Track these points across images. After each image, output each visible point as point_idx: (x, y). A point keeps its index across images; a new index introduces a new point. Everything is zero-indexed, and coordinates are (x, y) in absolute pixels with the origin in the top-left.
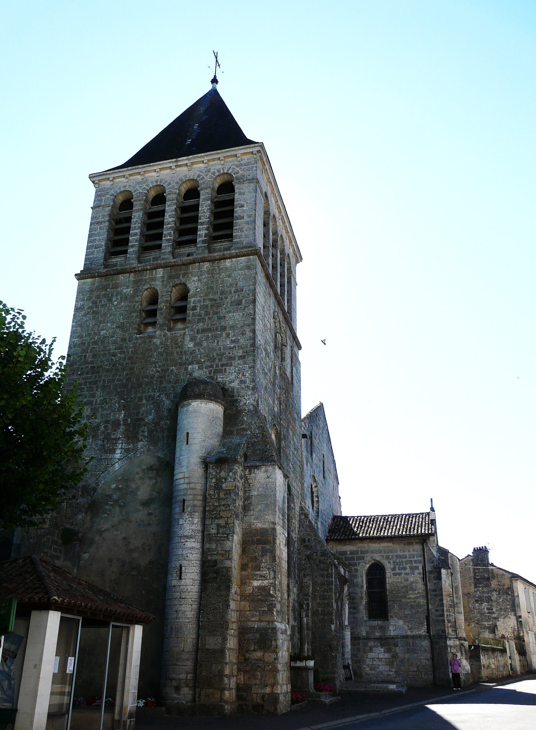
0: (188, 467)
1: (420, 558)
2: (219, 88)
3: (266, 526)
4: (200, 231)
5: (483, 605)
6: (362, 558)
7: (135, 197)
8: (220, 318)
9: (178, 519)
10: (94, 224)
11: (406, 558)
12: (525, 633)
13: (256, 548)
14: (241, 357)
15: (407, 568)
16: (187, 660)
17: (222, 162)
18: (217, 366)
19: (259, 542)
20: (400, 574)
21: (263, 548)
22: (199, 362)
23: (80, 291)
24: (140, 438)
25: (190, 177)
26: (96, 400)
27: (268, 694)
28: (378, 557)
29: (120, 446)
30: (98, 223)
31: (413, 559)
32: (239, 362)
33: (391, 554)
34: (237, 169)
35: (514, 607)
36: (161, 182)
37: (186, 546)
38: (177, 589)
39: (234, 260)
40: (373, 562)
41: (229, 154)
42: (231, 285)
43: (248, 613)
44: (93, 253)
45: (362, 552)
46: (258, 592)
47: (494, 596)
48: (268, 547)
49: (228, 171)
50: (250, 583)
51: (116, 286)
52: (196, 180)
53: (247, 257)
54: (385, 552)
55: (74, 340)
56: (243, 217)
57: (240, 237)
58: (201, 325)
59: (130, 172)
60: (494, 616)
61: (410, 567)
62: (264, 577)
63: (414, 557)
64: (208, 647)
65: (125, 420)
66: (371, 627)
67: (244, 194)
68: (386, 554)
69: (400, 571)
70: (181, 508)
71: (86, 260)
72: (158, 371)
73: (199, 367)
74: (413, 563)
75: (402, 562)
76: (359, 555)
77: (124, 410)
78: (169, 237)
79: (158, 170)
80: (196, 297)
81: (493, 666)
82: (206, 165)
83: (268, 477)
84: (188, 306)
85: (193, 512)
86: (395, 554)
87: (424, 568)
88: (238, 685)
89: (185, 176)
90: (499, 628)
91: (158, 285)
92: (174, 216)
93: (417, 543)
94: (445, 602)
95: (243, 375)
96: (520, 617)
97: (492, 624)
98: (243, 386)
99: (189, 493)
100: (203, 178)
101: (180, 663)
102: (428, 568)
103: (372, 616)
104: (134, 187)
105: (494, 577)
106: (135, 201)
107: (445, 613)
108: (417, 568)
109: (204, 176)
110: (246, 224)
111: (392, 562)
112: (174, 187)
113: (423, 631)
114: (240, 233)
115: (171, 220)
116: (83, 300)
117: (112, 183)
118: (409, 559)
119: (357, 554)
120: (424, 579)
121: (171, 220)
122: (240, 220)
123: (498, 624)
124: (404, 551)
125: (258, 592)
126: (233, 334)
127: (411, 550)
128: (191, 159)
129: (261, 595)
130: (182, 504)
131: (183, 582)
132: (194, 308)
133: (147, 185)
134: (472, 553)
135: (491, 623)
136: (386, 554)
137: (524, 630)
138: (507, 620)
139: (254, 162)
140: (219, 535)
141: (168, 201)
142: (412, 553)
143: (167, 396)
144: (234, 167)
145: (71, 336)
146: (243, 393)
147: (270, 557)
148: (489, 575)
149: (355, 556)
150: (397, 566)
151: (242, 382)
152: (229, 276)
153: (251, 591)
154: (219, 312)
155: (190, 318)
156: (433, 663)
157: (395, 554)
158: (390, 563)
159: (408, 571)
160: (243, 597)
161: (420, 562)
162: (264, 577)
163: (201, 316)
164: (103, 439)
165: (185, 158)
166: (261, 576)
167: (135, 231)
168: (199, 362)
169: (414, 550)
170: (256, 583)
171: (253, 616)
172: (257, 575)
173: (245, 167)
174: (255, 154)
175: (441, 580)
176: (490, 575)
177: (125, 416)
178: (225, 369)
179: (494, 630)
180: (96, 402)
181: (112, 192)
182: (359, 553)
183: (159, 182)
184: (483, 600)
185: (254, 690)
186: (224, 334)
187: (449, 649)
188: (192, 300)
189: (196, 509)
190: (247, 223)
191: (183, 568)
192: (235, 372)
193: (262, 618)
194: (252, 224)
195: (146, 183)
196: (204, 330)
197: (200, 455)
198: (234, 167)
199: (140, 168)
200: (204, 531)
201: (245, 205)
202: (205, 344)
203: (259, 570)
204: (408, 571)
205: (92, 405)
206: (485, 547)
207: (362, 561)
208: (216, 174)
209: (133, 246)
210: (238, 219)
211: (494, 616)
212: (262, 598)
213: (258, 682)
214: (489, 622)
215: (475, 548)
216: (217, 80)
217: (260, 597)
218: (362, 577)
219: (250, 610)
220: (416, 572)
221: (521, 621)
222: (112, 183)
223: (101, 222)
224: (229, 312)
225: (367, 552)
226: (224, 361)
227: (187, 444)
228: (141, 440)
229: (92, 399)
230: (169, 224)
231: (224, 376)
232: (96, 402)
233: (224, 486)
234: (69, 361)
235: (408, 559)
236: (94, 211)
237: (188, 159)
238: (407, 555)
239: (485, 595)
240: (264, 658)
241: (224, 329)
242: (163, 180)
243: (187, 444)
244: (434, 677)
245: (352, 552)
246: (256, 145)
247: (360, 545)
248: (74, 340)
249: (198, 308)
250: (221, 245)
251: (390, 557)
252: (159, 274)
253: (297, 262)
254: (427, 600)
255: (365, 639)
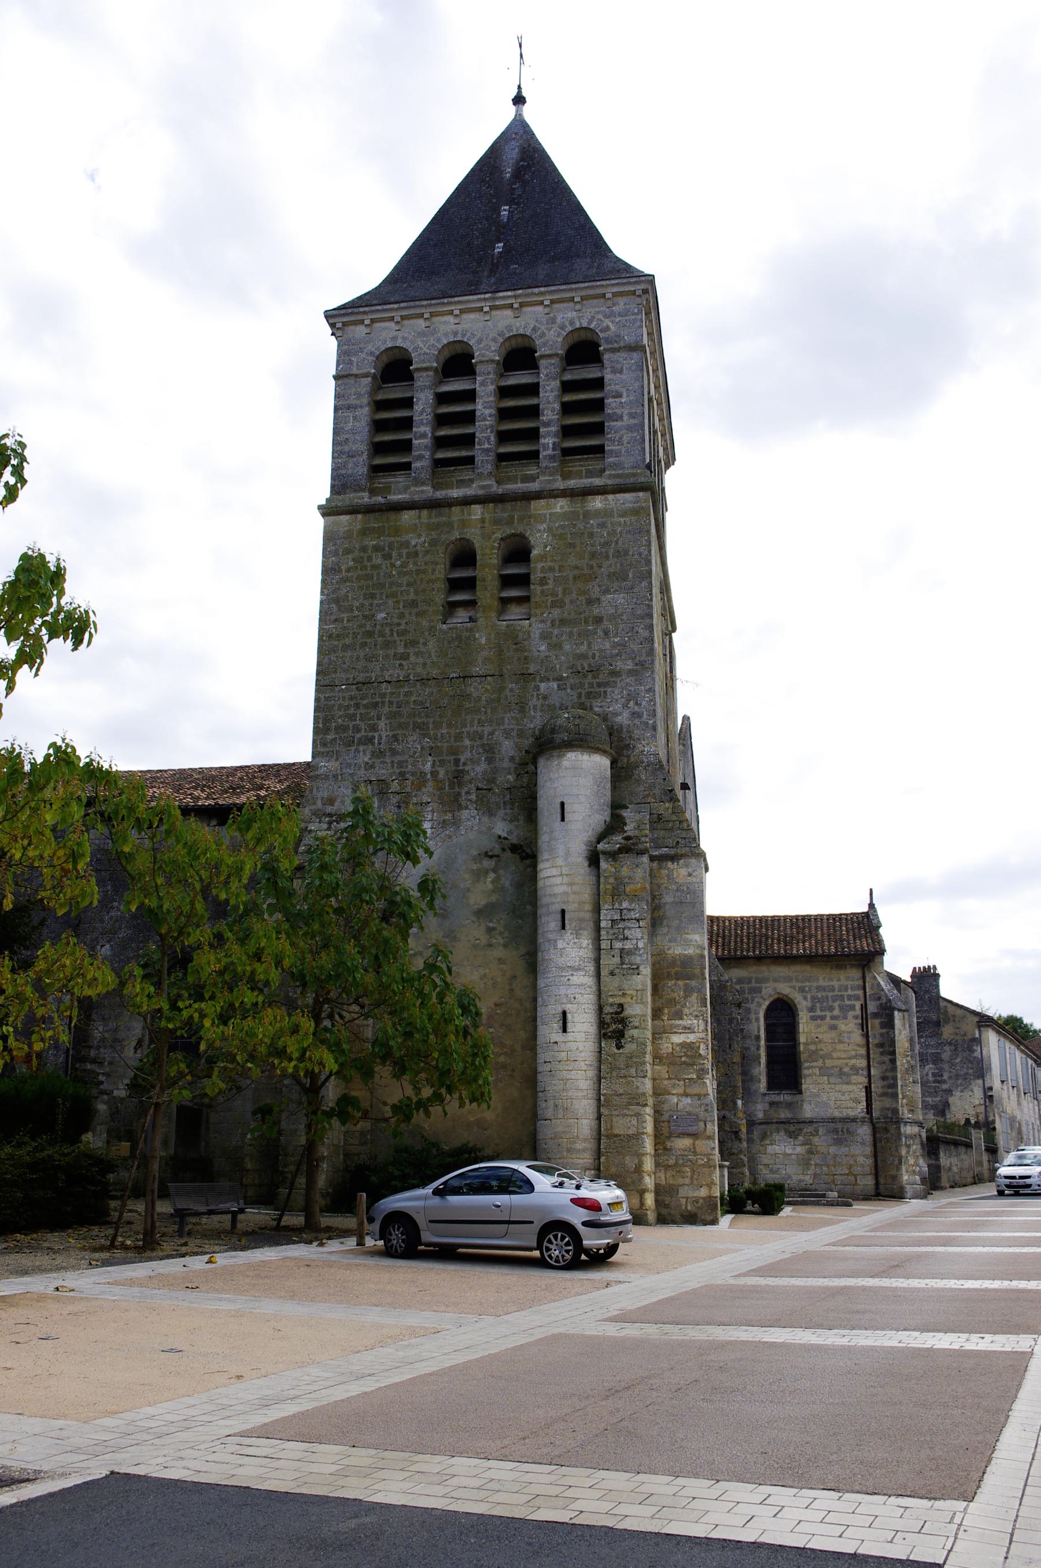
0: (566, 859)
1: (856, 992)
2: (530, 114)
3: (690, 951)
4: (545, 437)
5: (927, 1067)
6: (759, 990)
7: (416, 362)
8: (590, 602)
9: (555, 941)
10: (342, 409)
11: (833, 990)
12: (997, 1116)
13: (675, 985)
14: (630, 673)
15: (834, 1009)
16: (584, 1150)
17: (578, 307)
18: (591, 685)
19: (678, 977)
20: (823, 1018)
21: (686, 985)
22: (560, 679)
23: (329, 538)
24: (464, 803)
25: (517, 330)
26: (380, 735)
27: (704, 1199)
28: (785, 989)
29: (429, 817)
30: (349, 407)
31: (845, 993)
32: (628, 680)
33: (807, 984)
34: (607, 322)
35: (981, 1070)
36: (464, 335)
37: (571, 982)
38: (563, 1047)
39: (610, 497)
40: (776, 996)
41: (591, 292)
42: (607, 544)
43: (666, 1082)
44: (345, 465)
45: (758, 981)
46: (681, 1052)
47: (946, 1053)
48: (693, 983)
49: (590, 322)
50: (667, 1037)
51: (397, 531)
52: (529, 337)
53: (634, 494)
54: (797, 980)
55: (327, 627)
56: (621, 417)
57: (618, 454)
58: (556, 613)
59: (405, 313)
60: (945, 1086)
61: (839, 1006)
62: (689, 1028)
63: (846, 990)
64: (616, 1131)
65: (434, 774)
66: (772, 1104)
67: (621, 372)
68: (799, 985)
69: (823, 1014)
70: (560, 924)
71: (333, 478)
72: (487, 690)
73: (558, 686)
74: (846, 1000)
75: (827, 997)
76: (754, 985)
77: (430, 755)
78: (486, 446)
79: (457, 312)
80: (546, 561)
81: (955, 1169)
82: (547, 310)
83: (690, 875)
84: (532, 577)
85: (580, 929)
86: (815, 984)
87: (864, 1007)
88: (657, 1186)
89: (509, 328)
90: (953, 1108)
91: (474, 535)
92: (493, 404)
93: (852, 966)
94: (898, 1063)
95: (637, 704)
96: (991, 1089)
97: (940, 1101)
98: (637, 721)
99: (570, 899)
100: (543, 335)
101: (574, 1156)
102: (872, 1007)
103: (773, 1084)
104: (412, 342)
105: (947, 1021)
106: (417, 370)
107: (900, 1083)
108: (852, 1008)
109: (545, 331)
110: (627, 429)
111: (809, 997)
112: (490, 348)
113: (860, 1111)
114: (617, 448)
115: (487, 412)
116: (336, 553)
117: (367, 330)
118: (839, 993)
119: (750, 982)
120: (864, 1026)
121: (487, 412)
122: (615, 423)
123: (951, 1100)
124: (831, 980)
125: (681, 1052)
126: (615, 632)
127: (842, 977)
128: (519, 296)
129: (686, 1055)
130: (559, 916)
131: (569, 1036)
132: (543, 582)
133: (439, 340)
134: (911, 976)
135: (939, 1098)
136: (799, 985)
137: (996, 1110)
138: (968, 1093)
139: (636, 310)
140: (624, 966)
141: (480, 375)
142: (843, 982)
143: (507, 735)
144: (600, 317)
145: (320, 620)
146: (637, 733)
147: (697, 999)
148: (939, 1017)
149: (746, 986)
150: (818, 1005)
151: (636, 715)
152: (602, 525)
153: (670, 1050)
154: (588, 590)
155: (537, 599)
156: (876, 1161)
157: (815, 984)
158: (805, 998)
159: (836, 1012)
160: (657, 1058)
161: (857, 998)
162: (689, 1028)
163: (557, 596)
164: (399, 803)
165: (509, 293)
166: (685, 1028)
167: (422, 429)
168: (560, 679)
169: (847, 979)
170: (677, 1039)
171: (674, 1086)
172: (678, 1026)
173: (620, 318)
174: (639, 296)
175: (894, 1029)
176: (941, 1016)
177: (433, 765)
178: (605, 692)
179: (944, 1110)
180: (380, 738)
181: (370, 347)
182: (753, 981)
183: (459, 335)
184: (927, 1060)
185: (683, 1192)
186: (600, 632)
187: (904, 1139)
188: (540, 565)
189: (584, 925)
190: (630, 428)
191: (569, 1016)
192: (622, 697)
193: (688, 1091)
194: (638, 431)
195: (436, 336)
196: (563, 622)
197: (585, 839)
198: (600, 317)
199: (423, 306)
200: (600, 958)
201: (625, 395)
202: (567, 647)
203: (682, 1019)
204: (836, 1012)
205: (373, 744)
206: (935, 967)
207: (759, 995)
208: (567, 329)
209: (420, 457)
210: (614, 421)
211: (945, 1086)
212: (687, 1060)
213: (687, 1181)
214: (935, 1097)
215: (915, 968)
216: (524, 98)
217: (683, 1059)
218: (757, 1020)
219: (669, 1079)
220: (851, 1014)
221: (991, 1096)
222: (367, 330)
223: (355, 407)
224: (607, 591)
225: (766, 980)
226: (602, 678)
227: (563, 820)
228: (467, 808)
229: (370, 734)
230: (485, 420)
231: (603, 704)
232: (380, 738)
233: (628, 889)
234: (322, 665)
235: (836, 993)
236: (340, 382)
237: (515, 297)
238: (836, 986)
239: (930, 1051)
240: (694, 1148)
241: (598, 620)
242: (466, 331)
243: (563, 820)
244: (877, 1184)
245: (740, 981)
246: (643, 278)
247: (753, 969)
248: (327, 627)
249: (551, 582)
250: (582, 466)
251: (807, 989)
252: (475, 515)
253: (667, 467)
254: (869, 1062)
255: (761, 1123)
